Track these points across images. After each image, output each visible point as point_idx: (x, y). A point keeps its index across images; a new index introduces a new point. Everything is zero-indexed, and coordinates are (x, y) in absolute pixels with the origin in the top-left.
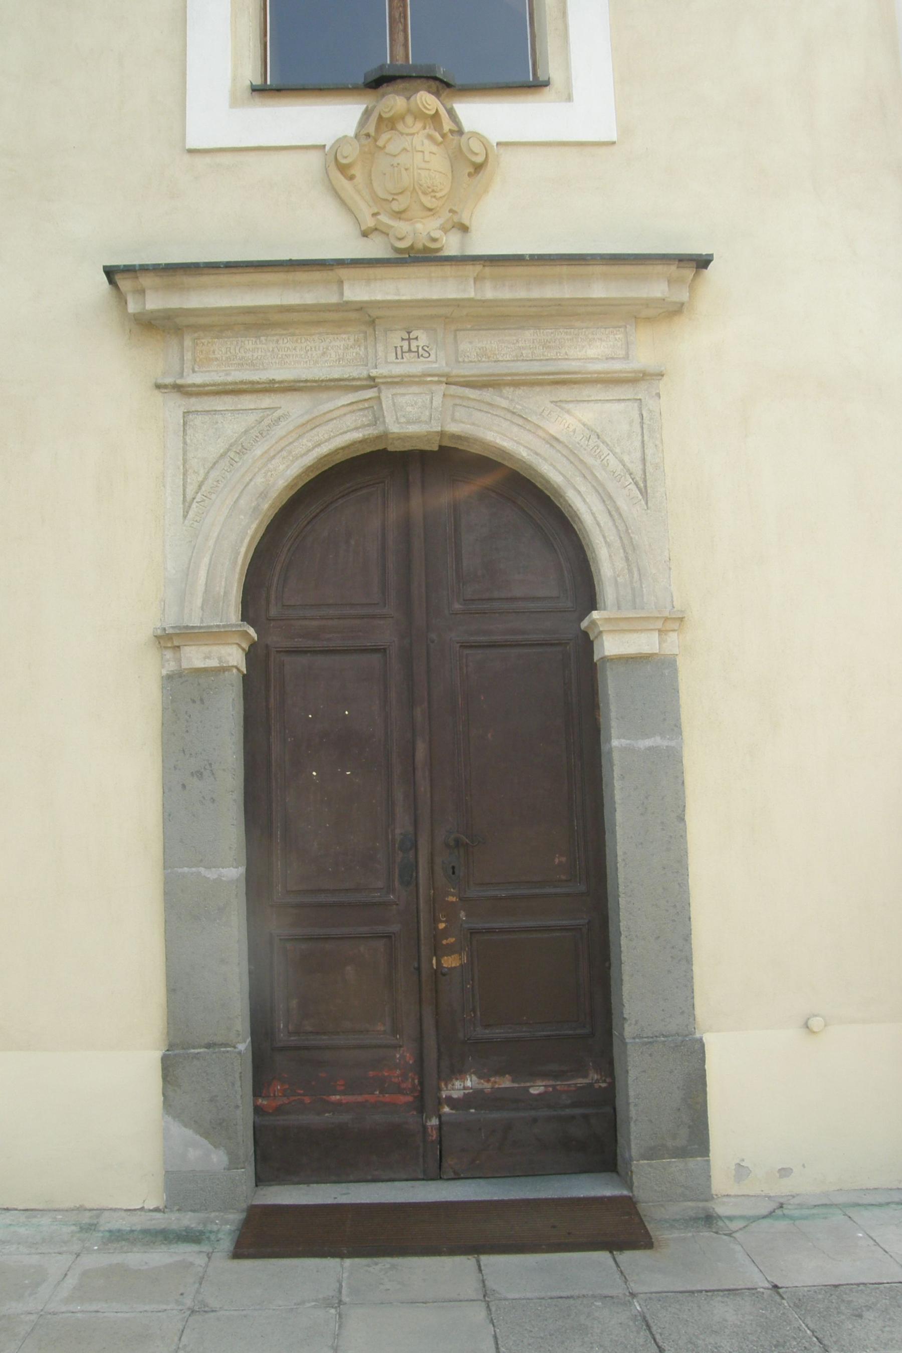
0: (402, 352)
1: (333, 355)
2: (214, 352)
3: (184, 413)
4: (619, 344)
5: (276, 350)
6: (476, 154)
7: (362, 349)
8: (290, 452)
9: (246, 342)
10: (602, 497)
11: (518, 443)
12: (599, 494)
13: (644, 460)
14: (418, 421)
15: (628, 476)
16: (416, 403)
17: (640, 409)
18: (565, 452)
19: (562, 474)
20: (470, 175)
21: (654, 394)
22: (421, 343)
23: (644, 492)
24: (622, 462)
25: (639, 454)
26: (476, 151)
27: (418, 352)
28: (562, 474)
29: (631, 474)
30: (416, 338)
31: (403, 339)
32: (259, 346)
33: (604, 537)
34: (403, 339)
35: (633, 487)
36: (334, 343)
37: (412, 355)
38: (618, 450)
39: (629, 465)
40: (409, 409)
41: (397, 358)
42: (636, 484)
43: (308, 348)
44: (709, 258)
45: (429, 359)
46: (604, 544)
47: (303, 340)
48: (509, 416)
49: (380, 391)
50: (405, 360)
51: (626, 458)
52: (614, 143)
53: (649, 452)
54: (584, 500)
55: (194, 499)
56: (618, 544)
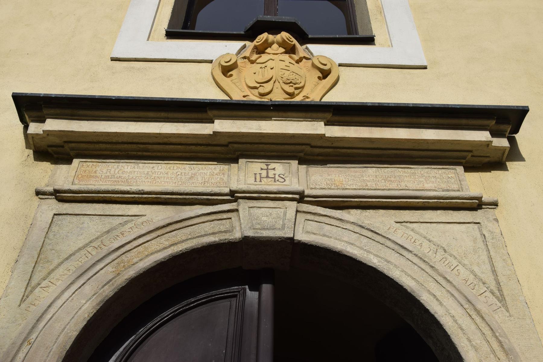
0: (261, 177)
1: (200, 179)
2: (95, 172)
3: (55, 215)
4: (453, 181)
5: (150, 173)
6: (325, 65)
7: (226, 176)
8: (146, 249)
9: (126, 167)
10: (458, 302)
11: (369, 252)
12: (456, 299)
13: (494, 272)
14: (273, 228)
15: (481, 284)
16: (271, 214)
17: (480, 231)
18: (416, 260)
19: (414, 279)
20: (319, 78)
21: (491, 219)
22: (277, 172)
23: (502, 299)
24: (472, 272)
25: (488, 267)
26: (325, 63)
27: (274, 178)
28: (414, 279)
29: (484, 283)
30: (274, 169)
31: (262, 169)
32: (136, 170)
33: (470, 341)
34: (262, 169)
35: (488, 294)
36: (201, 171)
37: (270, 179)
38: (466, 262)
39: (482, 276)
40: (264, 218)
41: (255, 181)
42: (493, 293)
43: (179, 173)
44: (526, 109)
45: (284, 183)
46: (470, 348)
47: (175, 168)
48: (357, 229)
49: (238, 205)
50: (263, 183)
51: (476, 269)
52: (425, 68)
53: (499, 265)
54: (441, 304)
55: (39, 284)
56: (485, 348)
